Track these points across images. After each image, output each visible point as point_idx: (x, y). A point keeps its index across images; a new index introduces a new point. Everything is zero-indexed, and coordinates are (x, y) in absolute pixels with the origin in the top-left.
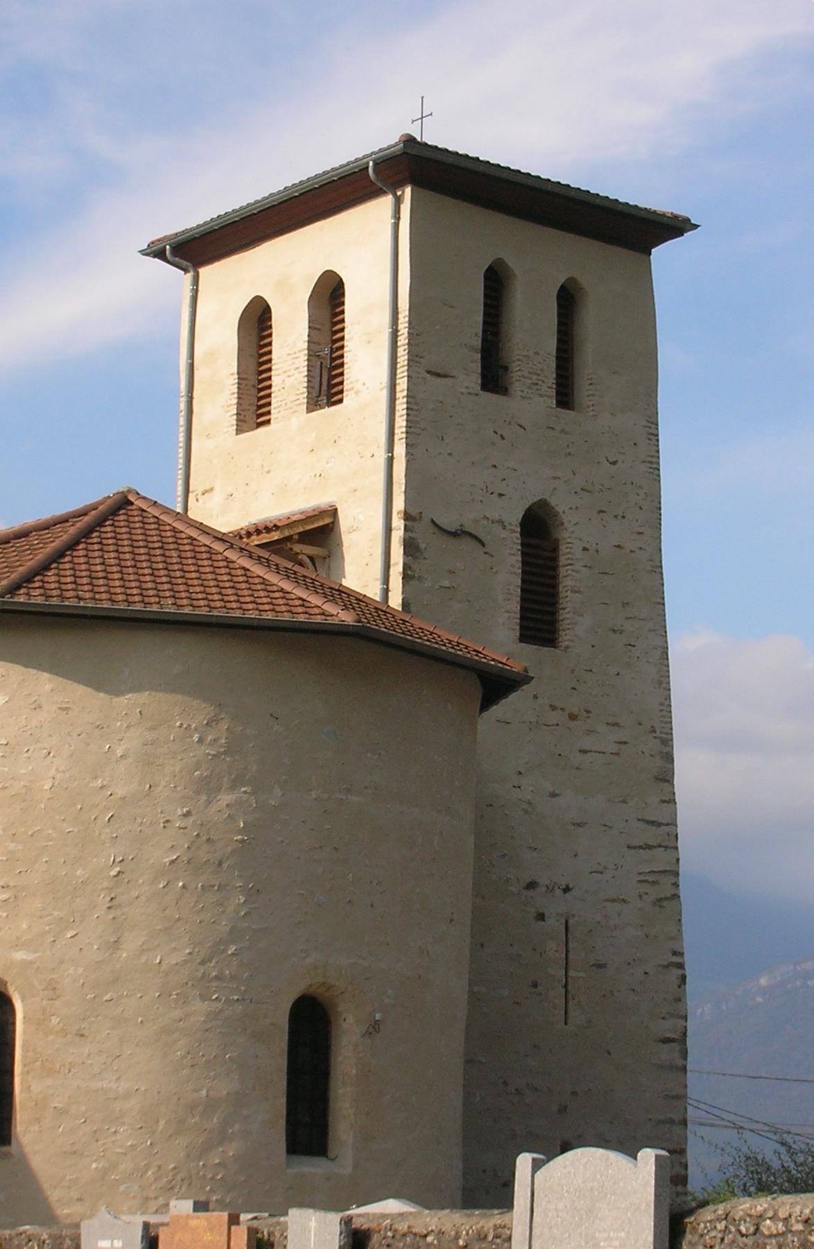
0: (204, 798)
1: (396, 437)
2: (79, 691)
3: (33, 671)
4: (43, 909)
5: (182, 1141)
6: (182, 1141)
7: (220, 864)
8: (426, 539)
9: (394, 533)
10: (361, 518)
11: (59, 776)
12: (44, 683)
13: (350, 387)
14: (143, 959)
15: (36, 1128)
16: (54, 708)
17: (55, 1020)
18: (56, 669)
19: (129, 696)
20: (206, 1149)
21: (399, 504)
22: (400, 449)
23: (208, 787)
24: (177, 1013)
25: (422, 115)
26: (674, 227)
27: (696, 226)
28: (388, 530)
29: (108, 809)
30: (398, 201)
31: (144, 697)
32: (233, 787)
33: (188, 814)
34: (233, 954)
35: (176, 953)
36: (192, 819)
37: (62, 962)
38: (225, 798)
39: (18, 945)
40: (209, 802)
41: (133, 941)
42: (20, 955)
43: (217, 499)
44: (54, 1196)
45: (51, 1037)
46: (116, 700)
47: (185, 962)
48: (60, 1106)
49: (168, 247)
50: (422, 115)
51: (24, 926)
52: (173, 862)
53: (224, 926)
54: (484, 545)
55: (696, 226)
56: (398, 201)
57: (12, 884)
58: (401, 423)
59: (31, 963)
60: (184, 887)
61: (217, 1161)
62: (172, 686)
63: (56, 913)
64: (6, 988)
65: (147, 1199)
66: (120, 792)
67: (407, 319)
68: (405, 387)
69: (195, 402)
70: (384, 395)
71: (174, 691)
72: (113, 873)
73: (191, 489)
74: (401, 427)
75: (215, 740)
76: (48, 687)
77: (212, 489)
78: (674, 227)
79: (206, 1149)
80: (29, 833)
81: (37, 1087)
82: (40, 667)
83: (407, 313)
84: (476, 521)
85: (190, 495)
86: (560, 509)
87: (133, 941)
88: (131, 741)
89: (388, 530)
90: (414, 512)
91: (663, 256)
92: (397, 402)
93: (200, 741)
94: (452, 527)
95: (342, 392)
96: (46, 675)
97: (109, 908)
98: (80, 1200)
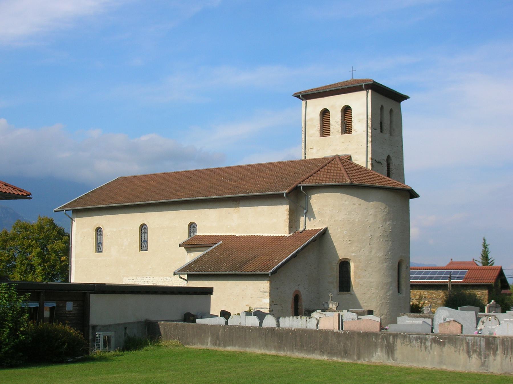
0: (385, 223)
1: (368, 142)
2: (362, 201)
3: (353, 197)
4: (357, 245)
5: (383, 291)
6: (383, 291)
7: (388, 236)
8: (375, 164)
9: (368, 162)
10: (358, 158)
11: (359, 218)
12: (356, 200)
13: (354, 130)
14: (376, 255)
15: (357, 289)
16: (358, 204)
17: (360, 267)
18: (358, 197)
19: (371, 202)
20: (387, 292)
21: (370, 156)
22: (370, 145)
23: (385, 221)
24: (382, 266)
25: (353, 72)
26: (405, 98)
27: (409, 98)
28: (367, 161)
29: (369, 225)
30: (367, 93)
31: (374, 203)
32: (389, 221)
33: (382, 226)
34: (390, 254)
35: (381, 254)
36: (383, 227)
37: (361, 256)
38: (388, 223)
39: (353, 252)
40: (385, 224)
41: (374, 251)
42: (353, 254)
43: (314, 150)
44: (361, 302)
45: (360, 271)
46: (369, 203)
47: (383, 256)
48: (362, 284)
49: (301, 95)
50: (353, 72)
51: (354, 248)
52: (380, 236)
53: (389, 248)
54: (382, 164)
55: (409, 98)
56: (367, 93)
57: (351, 240)
58: (370, 139)
59: (355, 256)
60: (382, 241)
61: (388, 294)
62: (378, 200)
63: (360, 246)
64: (349, 261)
65: (378, 302)
66: (371, 222)
67: (370, 118)
68: (371, 132)
69: (307, 129)
70: (365, 133)
71: (379, 201)
72: (370, 238)
73: (306, 147)
74: (369, 140)
75: (386, 211)
76: (357, 200)
77: (313, 148)
78: (405, 98)
79: (387, 292)
80: (354, 230)
81: (357, 280)
82: (354, 196)
83: (370, 116)
84: (381, 160)
85: (306, 149)
86: (391, 157)
87: (374, 251)
88: (372, 212)
89: (367, 161)
90: (372, 158)
91: (403, 104)
92: (368, 135)
93: (384, 211)
94: (378, 161)
95: (351, 132)
96: (356, 198)
97: (369, 245)
98: (366, 303)
